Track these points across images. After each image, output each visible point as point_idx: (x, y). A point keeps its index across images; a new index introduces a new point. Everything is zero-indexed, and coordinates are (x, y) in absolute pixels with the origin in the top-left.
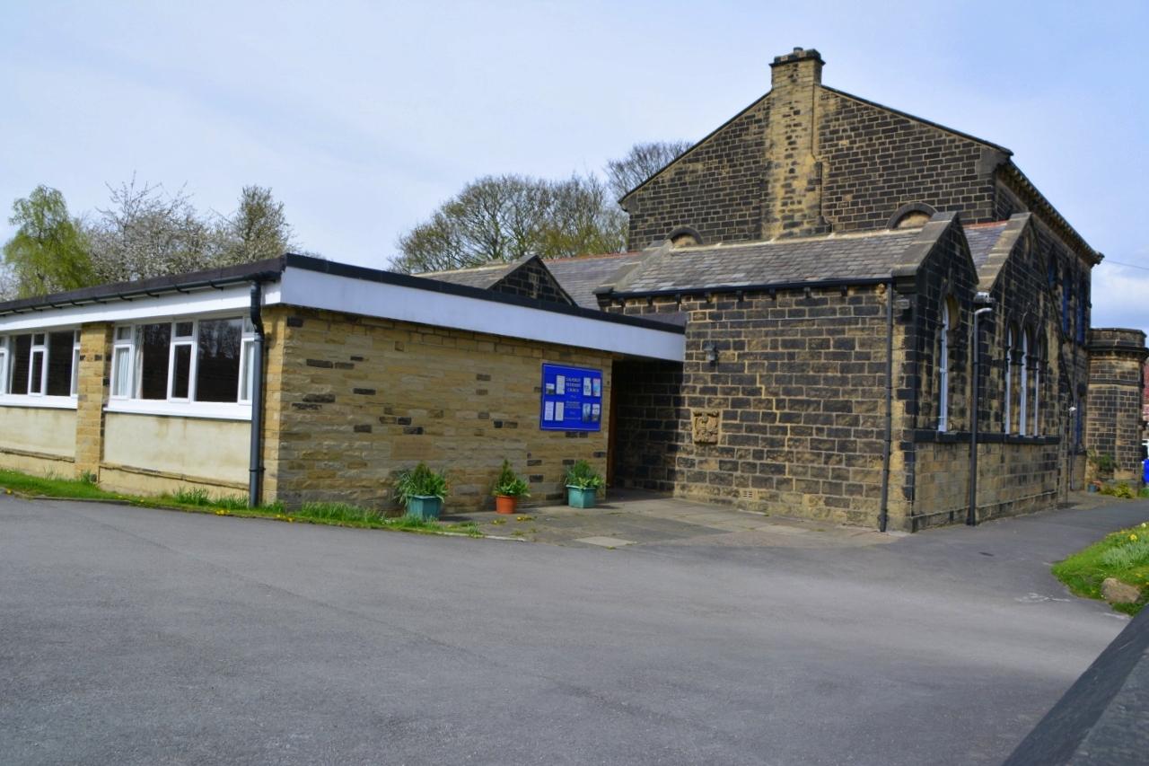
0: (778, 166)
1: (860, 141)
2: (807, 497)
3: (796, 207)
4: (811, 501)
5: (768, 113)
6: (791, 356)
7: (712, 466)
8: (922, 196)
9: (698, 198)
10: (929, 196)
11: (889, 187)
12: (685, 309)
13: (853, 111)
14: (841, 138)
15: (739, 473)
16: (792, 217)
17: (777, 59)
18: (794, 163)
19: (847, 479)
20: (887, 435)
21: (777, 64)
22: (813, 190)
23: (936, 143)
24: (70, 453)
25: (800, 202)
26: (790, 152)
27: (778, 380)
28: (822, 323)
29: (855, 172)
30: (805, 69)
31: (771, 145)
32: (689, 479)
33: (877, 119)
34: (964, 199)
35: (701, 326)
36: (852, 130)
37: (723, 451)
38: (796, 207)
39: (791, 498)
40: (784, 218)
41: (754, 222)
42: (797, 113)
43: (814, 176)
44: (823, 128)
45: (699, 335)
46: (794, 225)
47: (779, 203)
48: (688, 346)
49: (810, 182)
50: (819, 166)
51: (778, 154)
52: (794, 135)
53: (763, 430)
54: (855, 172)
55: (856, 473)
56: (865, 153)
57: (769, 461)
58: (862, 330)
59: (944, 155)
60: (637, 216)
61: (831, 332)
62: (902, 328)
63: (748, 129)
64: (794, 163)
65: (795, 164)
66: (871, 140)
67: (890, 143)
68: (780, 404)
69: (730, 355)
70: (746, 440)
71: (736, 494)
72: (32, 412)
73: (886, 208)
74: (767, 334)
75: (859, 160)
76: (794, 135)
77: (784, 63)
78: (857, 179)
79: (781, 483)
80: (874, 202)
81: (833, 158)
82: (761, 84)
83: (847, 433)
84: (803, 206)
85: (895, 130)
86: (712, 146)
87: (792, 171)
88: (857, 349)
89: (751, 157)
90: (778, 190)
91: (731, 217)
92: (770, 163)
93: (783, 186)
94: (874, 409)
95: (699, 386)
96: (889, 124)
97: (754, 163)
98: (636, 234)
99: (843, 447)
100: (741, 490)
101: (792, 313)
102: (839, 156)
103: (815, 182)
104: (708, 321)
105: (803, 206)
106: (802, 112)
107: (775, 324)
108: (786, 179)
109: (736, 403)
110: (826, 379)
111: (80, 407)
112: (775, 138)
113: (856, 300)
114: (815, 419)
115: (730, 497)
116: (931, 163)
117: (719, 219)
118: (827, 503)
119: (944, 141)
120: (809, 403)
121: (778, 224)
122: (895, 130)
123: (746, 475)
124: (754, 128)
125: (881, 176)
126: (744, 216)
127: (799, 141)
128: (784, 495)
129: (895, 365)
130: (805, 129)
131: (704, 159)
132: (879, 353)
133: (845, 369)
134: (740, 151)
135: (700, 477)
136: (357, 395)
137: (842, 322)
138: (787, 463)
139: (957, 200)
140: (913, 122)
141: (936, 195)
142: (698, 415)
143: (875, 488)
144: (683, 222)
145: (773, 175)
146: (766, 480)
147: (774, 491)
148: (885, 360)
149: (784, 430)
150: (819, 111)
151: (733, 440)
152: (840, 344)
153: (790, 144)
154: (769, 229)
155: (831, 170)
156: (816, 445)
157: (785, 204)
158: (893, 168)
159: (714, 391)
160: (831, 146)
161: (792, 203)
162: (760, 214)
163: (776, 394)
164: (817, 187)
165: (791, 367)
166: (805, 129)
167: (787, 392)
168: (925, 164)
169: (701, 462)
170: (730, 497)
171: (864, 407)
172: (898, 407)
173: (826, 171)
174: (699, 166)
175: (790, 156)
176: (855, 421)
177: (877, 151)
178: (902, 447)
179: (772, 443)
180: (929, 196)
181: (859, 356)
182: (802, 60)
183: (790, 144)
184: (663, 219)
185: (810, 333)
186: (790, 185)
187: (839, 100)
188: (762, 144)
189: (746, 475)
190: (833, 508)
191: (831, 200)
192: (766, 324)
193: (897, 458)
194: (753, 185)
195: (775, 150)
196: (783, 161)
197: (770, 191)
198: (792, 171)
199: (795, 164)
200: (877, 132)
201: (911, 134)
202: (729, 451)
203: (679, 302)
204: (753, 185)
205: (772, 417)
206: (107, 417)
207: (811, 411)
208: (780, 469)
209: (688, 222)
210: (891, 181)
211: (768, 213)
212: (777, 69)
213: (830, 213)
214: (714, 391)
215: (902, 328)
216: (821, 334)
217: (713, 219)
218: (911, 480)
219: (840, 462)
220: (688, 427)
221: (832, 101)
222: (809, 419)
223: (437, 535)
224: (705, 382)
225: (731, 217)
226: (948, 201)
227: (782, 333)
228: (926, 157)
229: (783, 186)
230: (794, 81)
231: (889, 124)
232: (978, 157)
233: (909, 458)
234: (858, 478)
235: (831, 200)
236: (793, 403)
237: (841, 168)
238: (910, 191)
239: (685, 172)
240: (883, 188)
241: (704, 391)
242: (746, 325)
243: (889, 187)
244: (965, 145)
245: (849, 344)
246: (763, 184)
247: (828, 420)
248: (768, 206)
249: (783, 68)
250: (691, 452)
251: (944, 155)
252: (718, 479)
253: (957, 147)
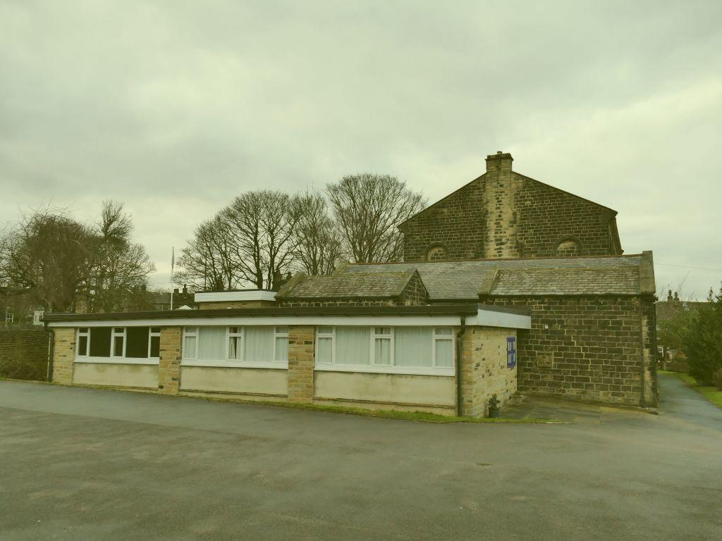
0: (492, 213)
1: (537, 203)
2: (601, 392)
3: (502, 235)
4: (604, 394)
5: (484, 185)
6: (589, 328)
7: (550, 378)
8: (572, 232)
9: (445, 227)
10: (576, 232)
11: (553, 227)
12: (529, 304)
13: (532, 187)
14: (527, 200)
15: (564, 381)
16: (501, 240)
17: (489, 157)
18: (501, 212)
19: (622, 384)
20: (641, 364)
21: (489, 159)
22: (512, 226)
23: (579, 206)
24: (285, 393)
25: (505, 232)
26: (498, 206)
27: (583, 338)
28: (605, 313)
29: (535, 218)
30: (504, 164)
31: (487, 202)
32: (537, 385)
33: (545, 192)
34: (594, 235)
35: (538, 312)
36: (532, 196)
37: (554, 371)
38: (502, 235)
39: (594, 393)
40: (497, 240)
41: (478, 241)
42: (502, 186)
43: (512, 219)
44: (516, 194)
45: (539, 317)
46: (502, 244)
47: (493, 232)
48: (533, 321)
49: (511, 222)
50: (514, 214)
51: (491, 207)
52: (500, 197)
53: (577, 361)
54: (535, 218)
55: (627, 381)
56: (540, 209)
57: (580, 376)
58: (626, 317)
59: (583, 212)
60: (409, 235)
61: (609, 317)
62: (646, 317)
63: (473, 192)
64: (501, 212)
65: (502, 214)
66: (543, 202)
67: (553, 204)
68: (585, 349)
69: (557, 327)
70: (567, 366)
71: (564, 391)
72: (232, 372)
73: (552, 237)
74: (576, 317)
75: (537, 212)
76: (500, 197)
77: (493, 159)
78: (536, 221)
79: (587, 386)
80: (546, 234)
81: (522, 210)
82: (480, 169)
83: (621, 363)
84: (507, 234)
85: (556, 198)
86: (452, 200)
87: (500, 216)
88: (624, 325)
89: (475, 207)
90: (491, 224)
91: (465, 238)
92: (487, 211)
93: (496, 224)
94: (634, 352)
95: (540, 340)
96: (552, 195)
97: (478, 210)
98: (409, 245)
99: (619, 369)
100: (566, 390)
101: (588, 308)
102: (525, 210)
103: (513, 222)
104: (543, 310)
105: (507, 234)
106: (505, 186)
107: (580, 312)
108: (497, 220)
109: (560, 349)
110: (608, 339)
111: (290, 368)
112: (489, 198)
113: (621, 303)
114: (604, 356)
115: (560, 393)
116: (576, 216)
117: (458, 239)
118: (613, 395)
119: (582, 205)
120: (600, 349)
121: (493, 243)
122: (556, 198)
123: (569, 382)
124: (476, 192)
125: (549, 221)
126: (473, 238)
127: (503, 200)
128: (590, 391)
129: (643, 333)
130: (507, 195)
131: (448, 207)
132: (635, 328)
133: (617, 334)
134: (469, 203)
135: (544, 384)
136: (307, 345)
137: (615, 313)
138: (590, 377)
139: (590, 235)
140: (565, 195)
141: (580, 232)
142: (539, 354)
143: (637, 388)
144: (437, 240)
145: (489, 217)
146: (580, 385)
147: (584, 390)
148: (638, 331)
149: (588, 362)
150: (514, 186)
151: (560, 366)
152: (614, 323)
153: (498, 202)
154: (488, 245)
155: (521, 216)
156: (605, 368)
157: (496, 233)
158: (555, 217)
159: (548, 343)
160: (521, 204)
161: (501, 233)
162: (482, 237)
163: (582, 345)
164: (514, 225)
165: (590, 333)
166: (507, 195)
167: (587, 344)
168: (573, 216)
169: (543, 377)
170: (560, 393)
171: (629, 351)
172: (646, 352)
173: (518, 217)
174: (445, 210)
175: (499, 208)
176: (625, 358)
177: (546, 208)
178: (649, 369)
179: (581, 367)
180: (576, 232)
181: (625, 328)
182: (502, 158)
183: (498, 202)
184: (424, 237)
185: (600, 317)
186: (499, 223)
187: (524, 180)
188: (482, 200)
189: (569, 382)
190: (616, 397)
191: (522, 232)
192: (576, 313)
193: (647, 375)
194: (478, 222)
195: (489, 204)
196: (494, 210)
197: (487, 226)
198: (500, 216)
199: (502, 214)
200: (546, 199)
201: (564, 201)
202: (559, 371)
203: (527, 300)
204: (478, 222)
205: (581, 356)
206: (320, 376)
207: (601, 353)
208: (587, 380)
209: (439, 240)
210: (554, 224)
211: (487, 237)
212: (490, 162)
213: (521, 239)
214: (548, 343)
215: (646, 317)
216: (605, 318)
217: (454, 239)
218: (654, 384)
219: (618, 376)
220: (535, 360)
221: (521, 181)
222: (601, 356)
223: (510, 422)
224: (543, 338)
225: (465, 238)
226: (585, 235)
227: (584, 317)
228: (573, 213)
229: (496, 224)
230: (499, 169)
231: (552, 195)
232: (601, 214)
233: (653, 375)
234: (628, 383)
235: (522, 232)
236: (592, 349)
237: (526, 216)
238: (566, 229)
239: (437, 213)
240: (550, 227)
241: (542, 343)
242: (564, 313)
243: (553, 227)
244: (593, 208)
245: (619, 323)
246: (483, 222)
247: (610, 357)
248: (487, 234)
249: (492, 162)
250: (537, 372)
251: (583, 212)
252: (551, 384)
253: (590, 208)
